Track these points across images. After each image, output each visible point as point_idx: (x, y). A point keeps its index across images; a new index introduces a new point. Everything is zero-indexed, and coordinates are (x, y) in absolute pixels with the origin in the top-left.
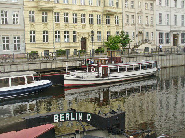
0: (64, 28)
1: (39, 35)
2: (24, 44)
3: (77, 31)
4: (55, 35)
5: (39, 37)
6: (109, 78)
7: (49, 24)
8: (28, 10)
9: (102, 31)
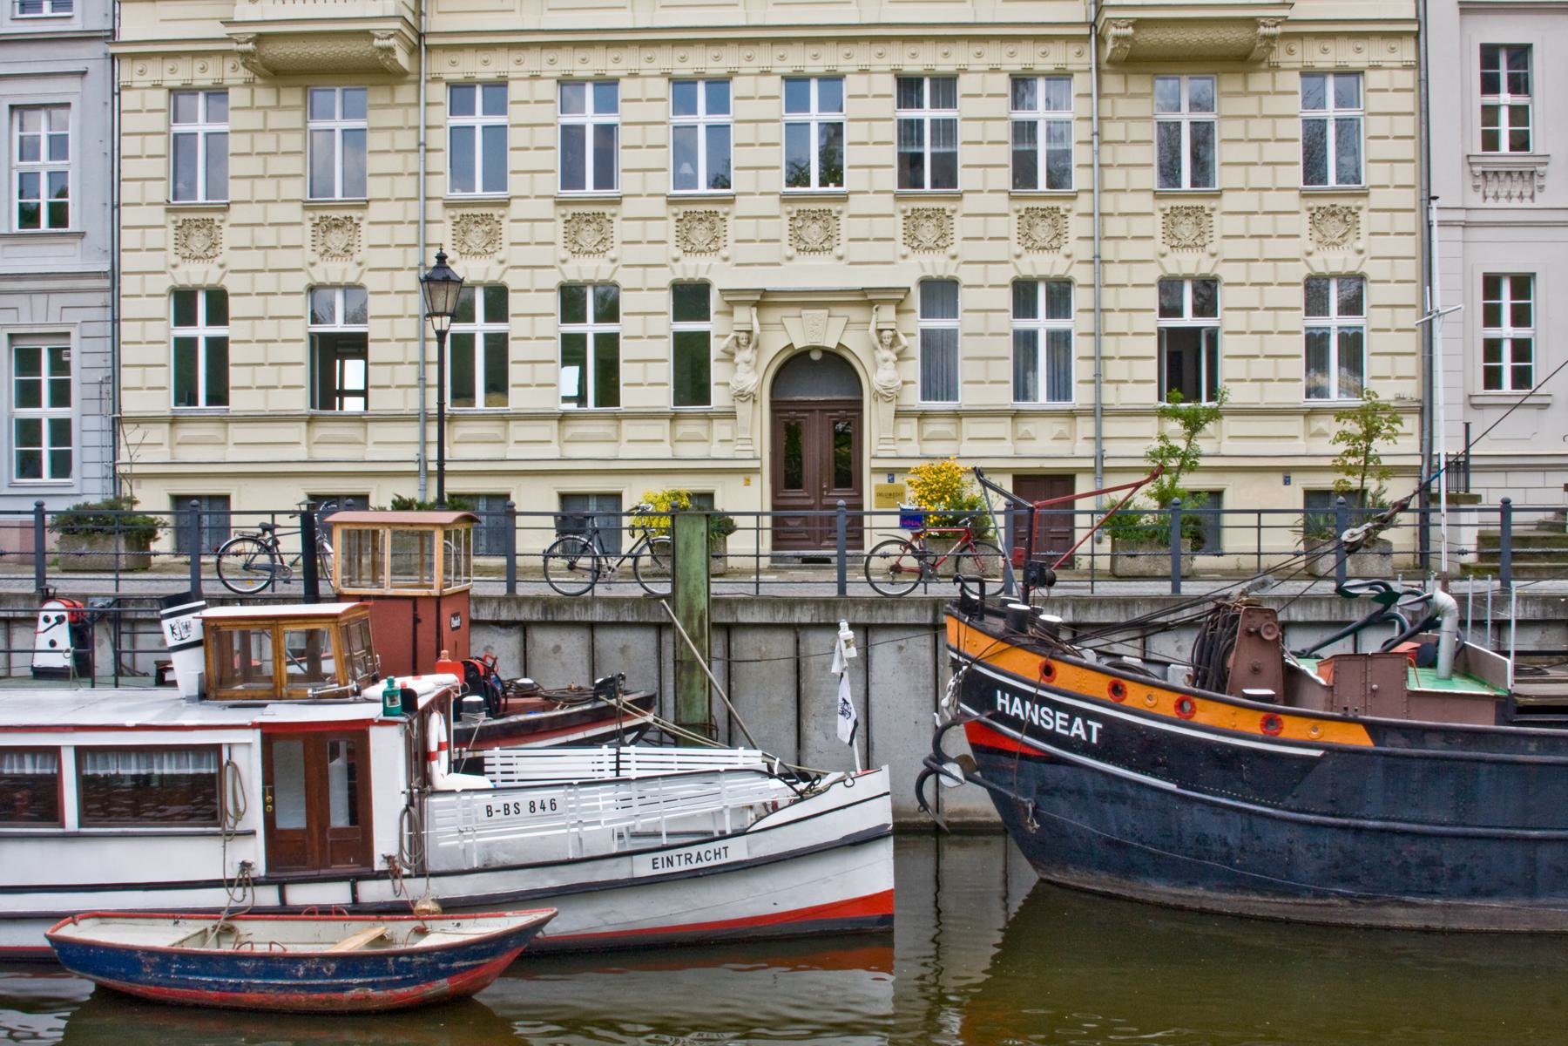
0: (1159, 245)
1: (266, 329)
2: (107, 425)
3: (721, 276)
4: (1077, 323)
5: (269, 368)
6: (372, 891)
7: (970, 204)
8: (156, 86)
9: (1081, 275)
